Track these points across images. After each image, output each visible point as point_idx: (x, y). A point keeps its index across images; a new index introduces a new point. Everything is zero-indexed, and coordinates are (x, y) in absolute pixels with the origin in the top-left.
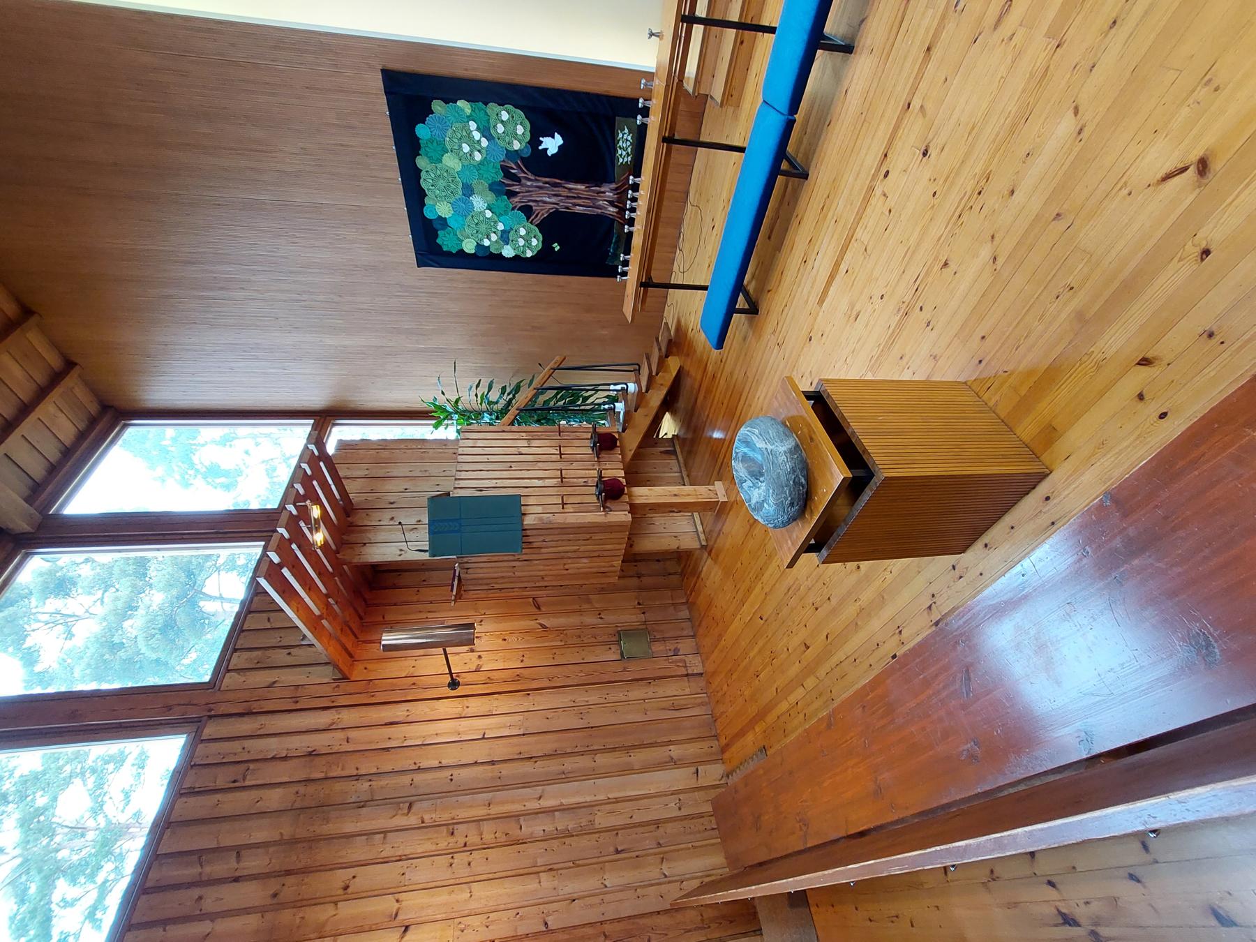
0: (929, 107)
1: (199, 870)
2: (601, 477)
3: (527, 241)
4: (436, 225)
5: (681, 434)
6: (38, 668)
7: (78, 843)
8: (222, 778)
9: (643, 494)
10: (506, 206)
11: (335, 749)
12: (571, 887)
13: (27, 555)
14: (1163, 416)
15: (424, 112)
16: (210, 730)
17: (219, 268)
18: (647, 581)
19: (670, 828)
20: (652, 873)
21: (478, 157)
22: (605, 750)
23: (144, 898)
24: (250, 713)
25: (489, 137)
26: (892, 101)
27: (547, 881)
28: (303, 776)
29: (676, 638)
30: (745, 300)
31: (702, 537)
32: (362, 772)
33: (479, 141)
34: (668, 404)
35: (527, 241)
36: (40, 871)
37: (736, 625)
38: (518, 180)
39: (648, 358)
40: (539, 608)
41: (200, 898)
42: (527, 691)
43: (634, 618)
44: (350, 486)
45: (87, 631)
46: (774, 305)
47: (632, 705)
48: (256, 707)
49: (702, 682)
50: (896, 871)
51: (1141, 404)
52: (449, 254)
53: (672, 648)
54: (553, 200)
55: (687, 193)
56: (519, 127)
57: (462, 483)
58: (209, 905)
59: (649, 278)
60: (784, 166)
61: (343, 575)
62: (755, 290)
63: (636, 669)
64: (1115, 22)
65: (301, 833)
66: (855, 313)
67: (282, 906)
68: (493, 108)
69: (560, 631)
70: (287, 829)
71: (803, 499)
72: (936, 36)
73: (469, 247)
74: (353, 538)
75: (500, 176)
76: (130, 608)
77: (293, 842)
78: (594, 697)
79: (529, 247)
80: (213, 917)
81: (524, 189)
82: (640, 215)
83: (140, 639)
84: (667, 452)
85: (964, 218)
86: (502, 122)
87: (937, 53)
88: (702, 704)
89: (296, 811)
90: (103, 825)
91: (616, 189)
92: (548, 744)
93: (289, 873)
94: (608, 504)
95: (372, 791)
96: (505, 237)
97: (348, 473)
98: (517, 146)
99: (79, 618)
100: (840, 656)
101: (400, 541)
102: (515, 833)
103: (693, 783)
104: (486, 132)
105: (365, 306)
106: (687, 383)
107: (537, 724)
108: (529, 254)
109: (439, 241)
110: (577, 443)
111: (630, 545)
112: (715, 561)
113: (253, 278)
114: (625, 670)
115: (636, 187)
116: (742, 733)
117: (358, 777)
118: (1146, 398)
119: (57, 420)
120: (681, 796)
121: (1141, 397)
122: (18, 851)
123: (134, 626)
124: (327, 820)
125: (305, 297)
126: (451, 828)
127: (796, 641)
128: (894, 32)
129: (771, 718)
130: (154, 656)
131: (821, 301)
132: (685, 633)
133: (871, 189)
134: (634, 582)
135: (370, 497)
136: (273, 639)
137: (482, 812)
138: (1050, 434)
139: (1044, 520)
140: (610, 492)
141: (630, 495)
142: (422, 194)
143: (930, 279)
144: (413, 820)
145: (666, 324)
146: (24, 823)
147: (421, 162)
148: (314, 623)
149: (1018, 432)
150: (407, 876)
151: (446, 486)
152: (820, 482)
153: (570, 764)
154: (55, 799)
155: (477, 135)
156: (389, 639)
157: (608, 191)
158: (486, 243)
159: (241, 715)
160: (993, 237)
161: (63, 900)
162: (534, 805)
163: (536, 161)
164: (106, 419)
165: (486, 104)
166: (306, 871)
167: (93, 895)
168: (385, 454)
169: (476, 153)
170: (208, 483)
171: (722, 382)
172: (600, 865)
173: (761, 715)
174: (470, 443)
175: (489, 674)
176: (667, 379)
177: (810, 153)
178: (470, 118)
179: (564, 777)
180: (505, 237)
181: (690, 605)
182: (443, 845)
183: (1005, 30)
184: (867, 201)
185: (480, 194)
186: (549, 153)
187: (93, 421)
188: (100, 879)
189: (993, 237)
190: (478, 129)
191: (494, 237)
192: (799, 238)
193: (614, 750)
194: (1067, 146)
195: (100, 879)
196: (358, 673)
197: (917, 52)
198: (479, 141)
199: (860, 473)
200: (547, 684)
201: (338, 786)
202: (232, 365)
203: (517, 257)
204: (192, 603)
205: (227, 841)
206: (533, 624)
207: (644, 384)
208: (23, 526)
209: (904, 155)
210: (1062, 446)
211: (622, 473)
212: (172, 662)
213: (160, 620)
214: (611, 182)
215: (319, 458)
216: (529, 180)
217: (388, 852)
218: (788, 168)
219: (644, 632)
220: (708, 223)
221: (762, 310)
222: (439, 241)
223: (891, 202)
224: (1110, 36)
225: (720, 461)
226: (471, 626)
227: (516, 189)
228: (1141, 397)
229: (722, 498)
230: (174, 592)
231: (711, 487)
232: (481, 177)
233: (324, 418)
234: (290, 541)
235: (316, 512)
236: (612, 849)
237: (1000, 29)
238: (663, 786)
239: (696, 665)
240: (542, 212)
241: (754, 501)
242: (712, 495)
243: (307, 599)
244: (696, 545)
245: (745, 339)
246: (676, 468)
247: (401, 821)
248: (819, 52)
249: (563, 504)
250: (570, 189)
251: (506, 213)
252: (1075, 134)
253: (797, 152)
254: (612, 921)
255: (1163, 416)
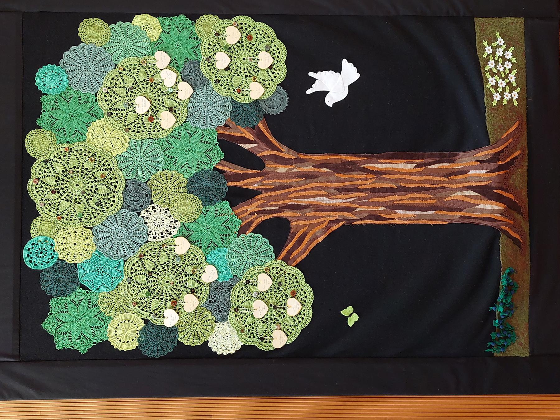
4: (47, 286)
52: (71, 356)
54: (340, 201)
68: (208, 23)
73: (124, 335)
81: (271, 183)
86: (228, 49)
91: (495, 157)
98: (256, 92)
104: (190, 73)
108: (279, 340)
109: (48, 325)
155: (169, 78)
158: (170, 319)
163: (300, 122)
165: (194, 17)
178: (158, 45)
180: (219, 301)
186: (330, 101)
190: (173, 65)
191: (190, 303)
203: (247, 352)
214: (478, 146)
216: (284, 162)
222: (48, 325)
227: (253, 183)
240: (312, 231)
248: (522, 20)
250: (378, 173)
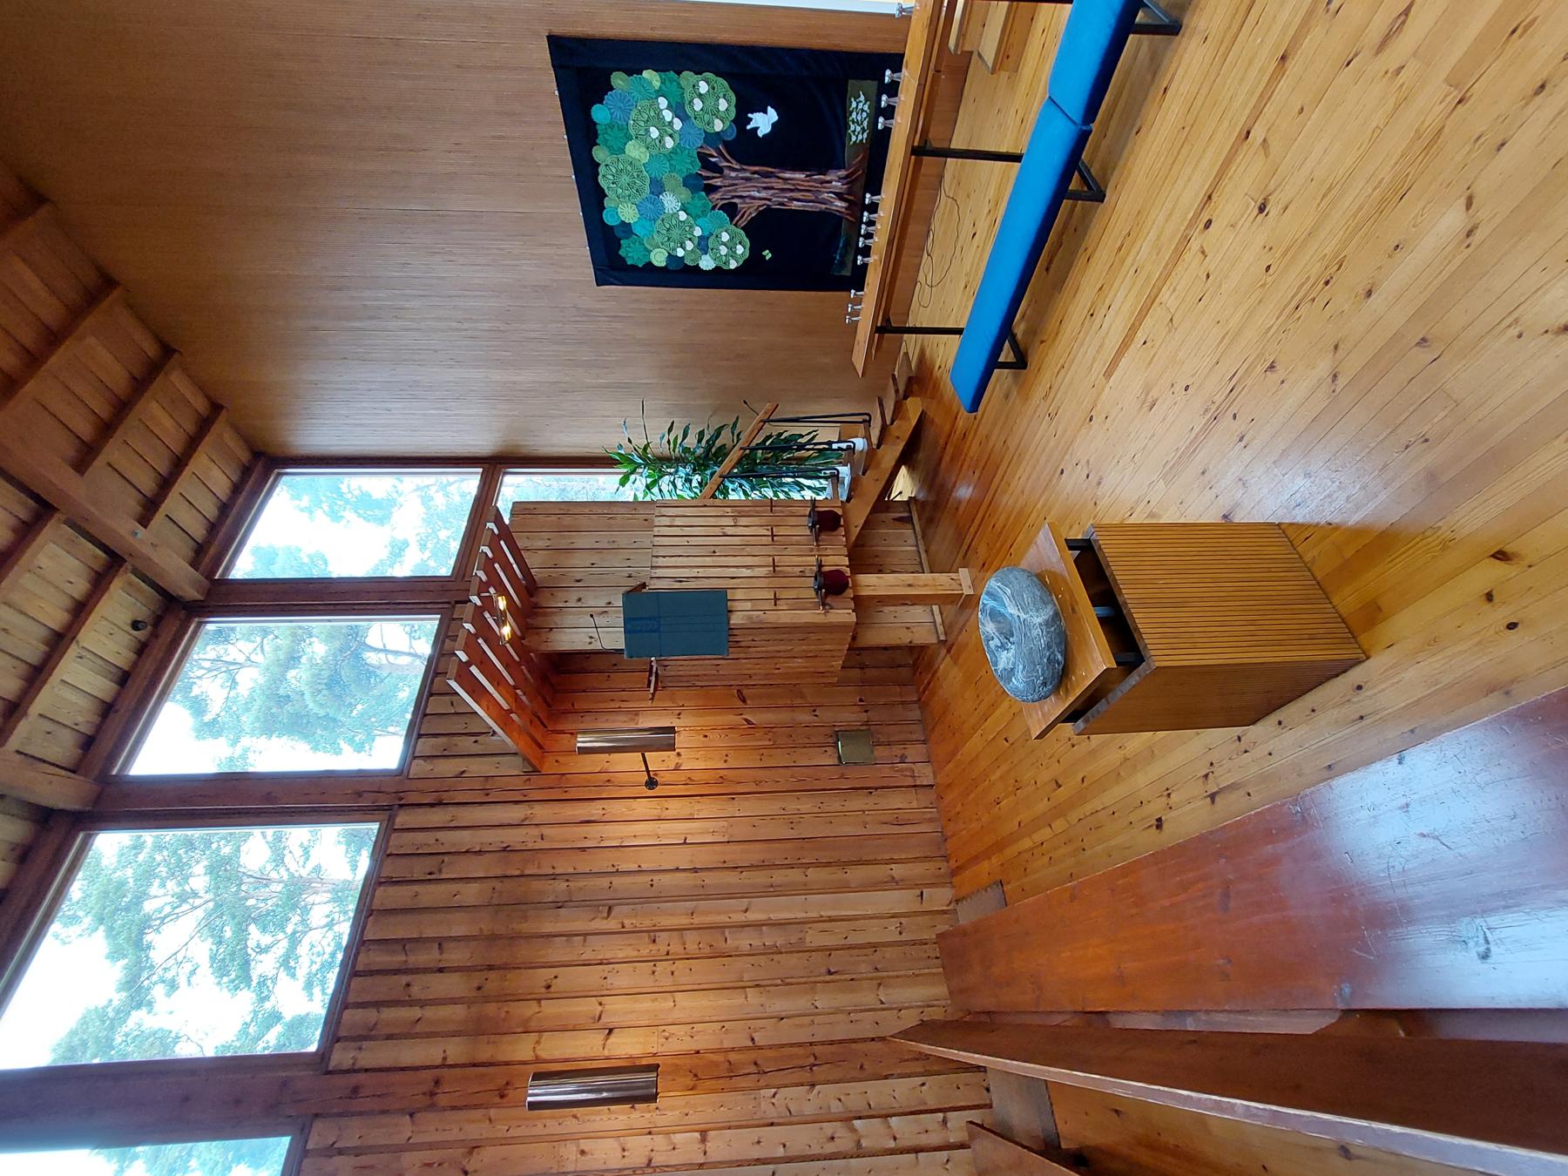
0: (1274, 144)
1: (404, 958)
2: (820, 566)
3: (730, 249)
4: (618, 233)
5: (920, 496)
6: (208, 718)
7: (264, 892)
8: (419, 869)
9: (871, 584)
10: (704, 206)
11: (530, 846)
12: (780, 1005)
13: (200, 624)
14: (1512, 626)
15: (599, 89)
16: (403, 819)
17: (367, 293)
18: (872, 673)
19: (889, 953)
20: (867, 998)
21: (669, 143)
22: (818, 865)
23: (356, 981)
24: (440, 804)
25: (683, 117)
26: (1226, 124)
27: (754, 997)
28: (499, 873)
29: (904, 742)
30: (1013, 349)
31: (941, 629)
32: (558, 871)
33: (671, 123)
34: (906, 458)
35: (730, 249)
36: (234, 917)
37: (975, 743)
38: (719, 170)
39: (881, 405)
40: (744, 701)
41: (408, 985)
42: (732, 795)
43: (853, 717)
44: (532, 560)
45: (249, 679)
46: (1049, 360)
47: (850, 816)
48: (446, 797)
49: (931, 795)
50: (1119, 1092)
51: (1488, 606)
52: (634, 267)
53: (899, 753)
55: (942, 177)
56: (722, 101)
57: (659, 572)
58: (416, 991)
59: (887, 319)
60: (1074, 185)
61: (526, 655)
62: (1025, 333)
63: (856, 776)
64: (1543, 87)
65: (500, 929)
66: (1150, 400)
67: (487, 1000)
69: (769, 729)
70: (485, 924)
71: (1061, 676)
72: (1296, 40)
73: (659, 259)
74: (538, 621)
75: (697, 168)
76: (293, 659)
77: (493, 938)
78: (806, 805)
79: (733, 255)
80: (423, 1004)
82: (879, 242)
83: (307, 696)
84: (900, 520)
85: (1302, 310)
86: (700, 96)
87: (1293, 66)
88: (931, 820)
89: (496, 907)
90: (286, 877)
91: (847, 177)
92: (755, 854)
93: (491, 968)
94: (828, 600)
95: (569, 891)
96: (703, 245)
97: (528, 544)
98: (718, 126)
99: (242, 666)
100: (1096, 804)
101: (591, 626)
102: (720, 945)
103: (917, 907)
104: (679, 110)
105: (533, 335)
106: (929, 434)
107: (741, 832)
108: (733, 265)
110: (793, 521)
111: (854, 638)
112: (955, 661)
113: (407, 305)
114: (842, 776)
115: (873, 208)
116: (976, 859)
117: (554, 877)
118: (1496, 599)
119: (210, 476)
120: (903, 920)
121: (1489, 597)
122: (210, 896)
123: (298, 677)
124: (525, 918)
125: (466, 325)
126: (652, 935)
127: (1045, 776)
128: (1239, 18)
129: (1010, 852)
130: (322, 713)
131: (1108, 374)
132: (914, 737)
133: (1187, 239)
134: (855, 673)
135: (554, 573)
136: (457, 725)
137: (684, 921)
138: (1373, 614)
139: (1352, 711)
140: (831, 585)
141: (855, 585)
142: (601, 194)
143: (1249, 382)
144: (612, 924)
145: (906, 354)
146: (211, 870)
147: (599, 154)
148: (503, 718)
149: (1335, 600)
150: (609, 981)
151: (643, 575)
152: (1079, 660)
153: (779, 877)
154: (238, 850)
155: (668, 115)
156: (583, 741)
157: (835, 180)
158: (680, 253)
159: (432, 805)
160: (1336, 347)
161: (258, 946)
162: (739, 918)
163: (744, 146)
164: (259, 468)
165: (679, 73)
166: (505, 967)
167: (284, 944)
168: (567, 520)
169: (668, 139)
170: (359, 515)
171: (975, 446)
172: (811, 986)
173: (1000, 846)
174: (666, 521)
175: (689, 774)
176: (904, 429)
177: (1109, 167)
178: (660, 93)
179: (772, 891)
180: (703, 245)
181: (922, 704)
182: (644, 952)
183: (1392, 58)
184: (1178, 254)
185: (673, 191)
186: (760, 134)
187: (246, 471)
188: (290, 929)
189: (1336, 347)
190: (669, 107)
191: (689, 246)
192: (1088, 280)
193: (828, 864)
194: (1449, 249)
195: (290, 929)
196: (549, 766)
197: (1265, 58)
198: (671, 123)
199: (1130, 657)
200: (753, 788)
201: (536, 885)
202: (389, 405)
203: (717, 268)
204: (357, 656)
205: (430, 933)
206: (737, 719)
207: (875, 440)
208: (191, 593)
209: (1233, 204)
210: (1387, 630)
211: (846, 561)
212: (340, 717)
213: (326, 674)
214: (839, 168)
215: (500, 537)
217: (588, 955)
218: (1080, 184)
219: (864, 733)
220: (967, 229)
221: (1033, 361)
223: (1211, 264)
224: (1530, 109)
225: (967, 541)
226: (671, 730)
228: (1489, 597)
229: (967, 591)
230: (337, 644)
231: (953, 575)
232: (673, 169)
233: (494, 465)
234: (476, 636)
235: (502, 603)
236: (824, 970)
237: (1383, 57)
238: (880, 907)
239: (925, 774)
240: (749, 210)
241: (1001, 667)
242: (955, 586)
243: (496, 695)
244: (934, 641)
245: (1007, 397)
246: (912, 541)
247: (600, 924)
249: (776, 599)
251: (704, 213)
252: (1462, 236)
253: (1092, 162)
254: (823, 1043)
255: (1512, 626)
